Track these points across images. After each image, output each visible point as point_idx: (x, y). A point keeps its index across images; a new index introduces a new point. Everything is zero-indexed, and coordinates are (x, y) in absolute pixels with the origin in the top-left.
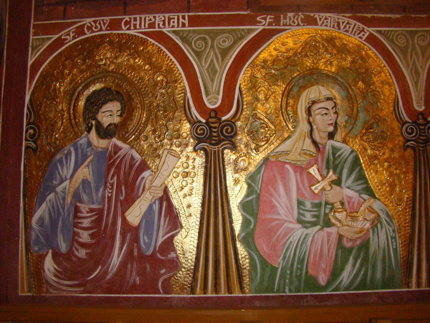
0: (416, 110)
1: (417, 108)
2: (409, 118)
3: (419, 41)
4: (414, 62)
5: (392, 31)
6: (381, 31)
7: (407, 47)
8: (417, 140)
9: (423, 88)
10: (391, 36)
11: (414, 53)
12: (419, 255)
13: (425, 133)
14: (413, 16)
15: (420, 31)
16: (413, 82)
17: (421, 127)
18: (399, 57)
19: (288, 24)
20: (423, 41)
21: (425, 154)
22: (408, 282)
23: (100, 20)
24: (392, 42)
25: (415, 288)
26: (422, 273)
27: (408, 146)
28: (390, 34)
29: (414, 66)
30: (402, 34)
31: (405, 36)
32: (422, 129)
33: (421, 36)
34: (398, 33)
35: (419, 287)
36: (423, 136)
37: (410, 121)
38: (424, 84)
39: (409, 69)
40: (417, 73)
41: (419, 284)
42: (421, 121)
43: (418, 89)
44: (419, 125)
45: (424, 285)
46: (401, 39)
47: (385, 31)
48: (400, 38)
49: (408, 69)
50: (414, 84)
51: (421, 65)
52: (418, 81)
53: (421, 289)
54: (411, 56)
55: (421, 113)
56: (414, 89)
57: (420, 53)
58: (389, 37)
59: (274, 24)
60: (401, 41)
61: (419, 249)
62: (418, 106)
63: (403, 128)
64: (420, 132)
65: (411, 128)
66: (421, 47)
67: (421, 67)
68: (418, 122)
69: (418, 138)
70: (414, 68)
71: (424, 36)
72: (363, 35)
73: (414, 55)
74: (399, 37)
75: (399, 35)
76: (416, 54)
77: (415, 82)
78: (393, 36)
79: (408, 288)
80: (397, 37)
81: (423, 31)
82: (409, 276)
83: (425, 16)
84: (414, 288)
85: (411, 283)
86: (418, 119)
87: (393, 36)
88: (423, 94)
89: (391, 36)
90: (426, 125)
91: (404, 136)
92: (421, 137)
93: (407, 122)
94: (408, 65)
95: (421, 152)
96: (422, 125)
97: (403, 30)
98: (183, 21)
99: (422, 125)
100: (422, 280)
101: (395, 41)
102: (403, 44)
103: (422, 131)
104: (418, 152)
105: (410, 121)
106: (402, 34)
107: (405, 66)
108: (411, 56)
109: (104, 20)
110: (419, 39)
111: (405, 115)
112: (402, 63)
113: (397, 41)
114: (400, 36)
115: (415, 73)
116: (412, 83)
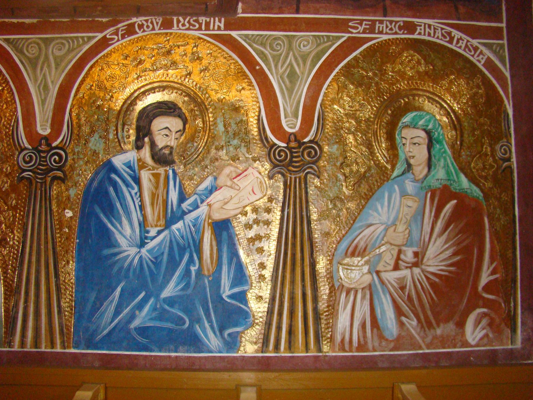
0: (40, 134)
1: (41, 132)
2: (30, 145)
3: (54, 50)
4: (45, 75)
5: (23, 38)
6: (10, 39)
7: (37, 58)
8: (36, 170)
9: (52, 106)
10: (21, 46)
11: (46, 65)
12: (26, 308)
13: (46, 161)
14: (53, 20)
15: (57, 38)
16: (40, 99)
17: (42, 155)
18: (26, 70)
19: (384, 32)
20: (60, 50)
21: (44, 186)
22: (11, 340)
23: (433, 37)
24: (20, 51)
25: (18, 348)
26: (28, 331)
27: (23, 177)
28: (20, 43)
29: (44, 81)
30: (35, 43)
31: (38, 44)
32: (44, 157)
33: (58, 44)
34: (29, 41)
35: (22, 347)
36: (43, 165)
37: (30, 147)
38: (53, 102)
39: (37, 85)
40: (46, 88)
41: (23, 344)
42: (44, 147)
43: (45, 110)
44: (40, 152)
45: (29, 346)
46: (32, 49)
47: (14, 39)
48: (32, 47)
49: (35, 86)
50: (40, 102)
51: (53, 79)
52: (46, 99)
53: (25, 350)
54: (42, 70)
55: (46, 138)
56: (39, 108)
57: (53, 65)
58: (18, 47)
59: (126, 36)
60: (32, 51)
61: (26, 301)
62: (42, 129)
63: (21, 156)
64: (40, 161)
65: (30, 156)
66: (55, 59)
67: (52, 82)
68: (40, 148)
69: (36, 168)
70: (43, 82)
71: (62, 44)
72: (482, 59)
73: (45, 68)
74: (30, 46)
75: (31, 43)
76: (49, 66)
77: (42, 100)
78: (23, 45)
79: (9, 347)
80: (28, 46)
81: (61, 38)
82: (12, 333)
83: (68, 20)
84: (16, 348)
85: (14, 342)
86: (40, 145)
87: (23, 45)
88: (51, 114)
89: (21, 46)
90: (48, 152)
91: (20, 165)
92: (41, 167)
93: (26, 149)
94: (36, 80)
95: (39, 184)
96: (43, 152)
97: (37, 38)
98: (219, 24)
99: (43, 152)
100: (27, 339)
101: (25, 52)
102: (34, 54)
103: (42, 159)
104: (34, 185)
105: (30, 147)
106: (35, 43)
107: (33, 81)
108: (42, 70)
109: (448, 42)
110: (55, 47)
111: (25, 141)
112: (29, 77)
113: (28, 51)
114: (32, 45)
115: (44, 89)
116: (38, 101)
